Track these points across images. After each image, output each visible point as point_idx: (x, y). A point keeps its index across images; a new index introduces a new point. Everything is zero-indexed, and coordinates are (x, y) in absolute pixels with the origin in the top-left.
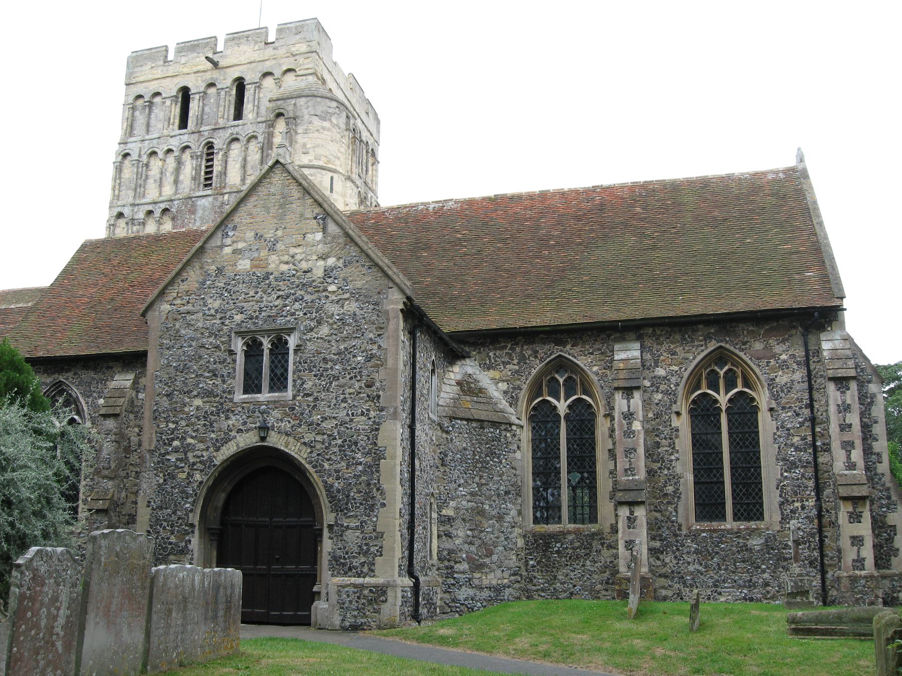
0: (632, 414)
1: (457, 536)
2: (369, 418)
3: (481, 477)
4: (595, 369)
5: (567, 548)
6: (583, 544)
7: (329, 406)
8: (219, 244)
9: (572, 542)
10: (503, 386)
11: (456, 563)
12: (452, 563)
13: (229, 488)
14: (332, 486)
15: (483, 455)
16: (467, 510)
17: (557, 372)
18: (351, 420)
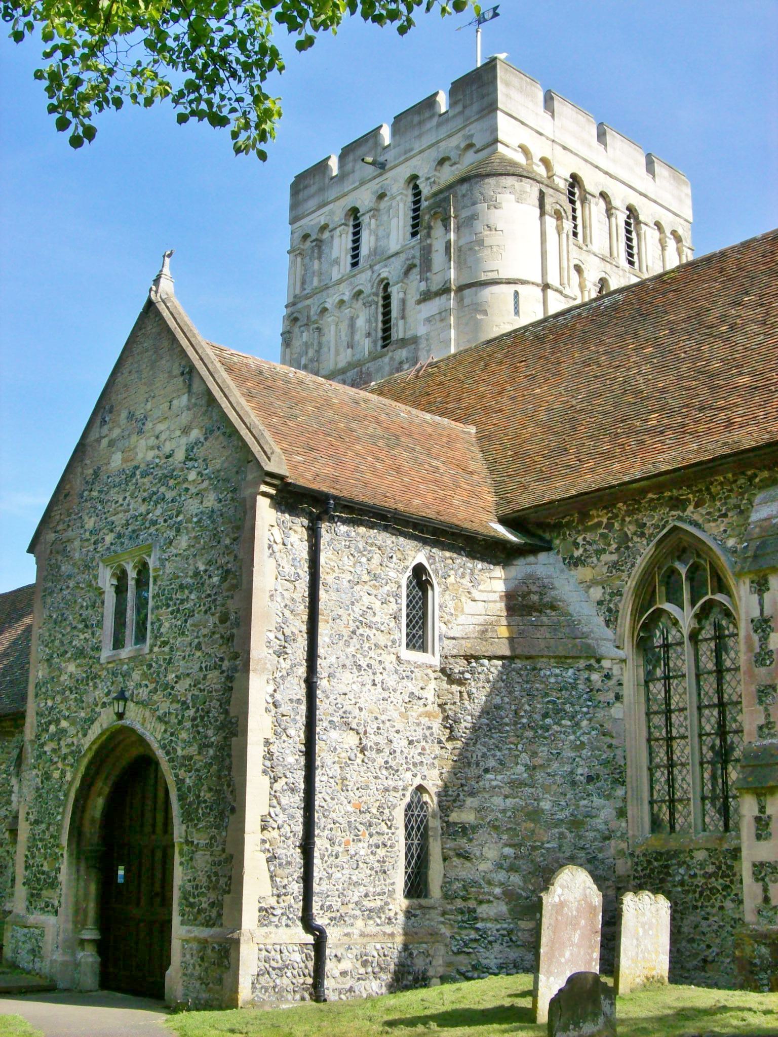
0: (766, 621)
1: (483, 858)
2: (222, 672)
3: (534, 754)
4: (731, 542)
5: (695, 875)
6: (719, 868)
7: (184, 658)
8: (97, 436)
9: (702, 865)
10: (597, 593)
11: (481, 902)
12: (472, 904)
13: (107, 790)
14: (183, 781)
15: (537, 717)
16: (504, 811)
17: (679, 558)
18: (205, 678)
